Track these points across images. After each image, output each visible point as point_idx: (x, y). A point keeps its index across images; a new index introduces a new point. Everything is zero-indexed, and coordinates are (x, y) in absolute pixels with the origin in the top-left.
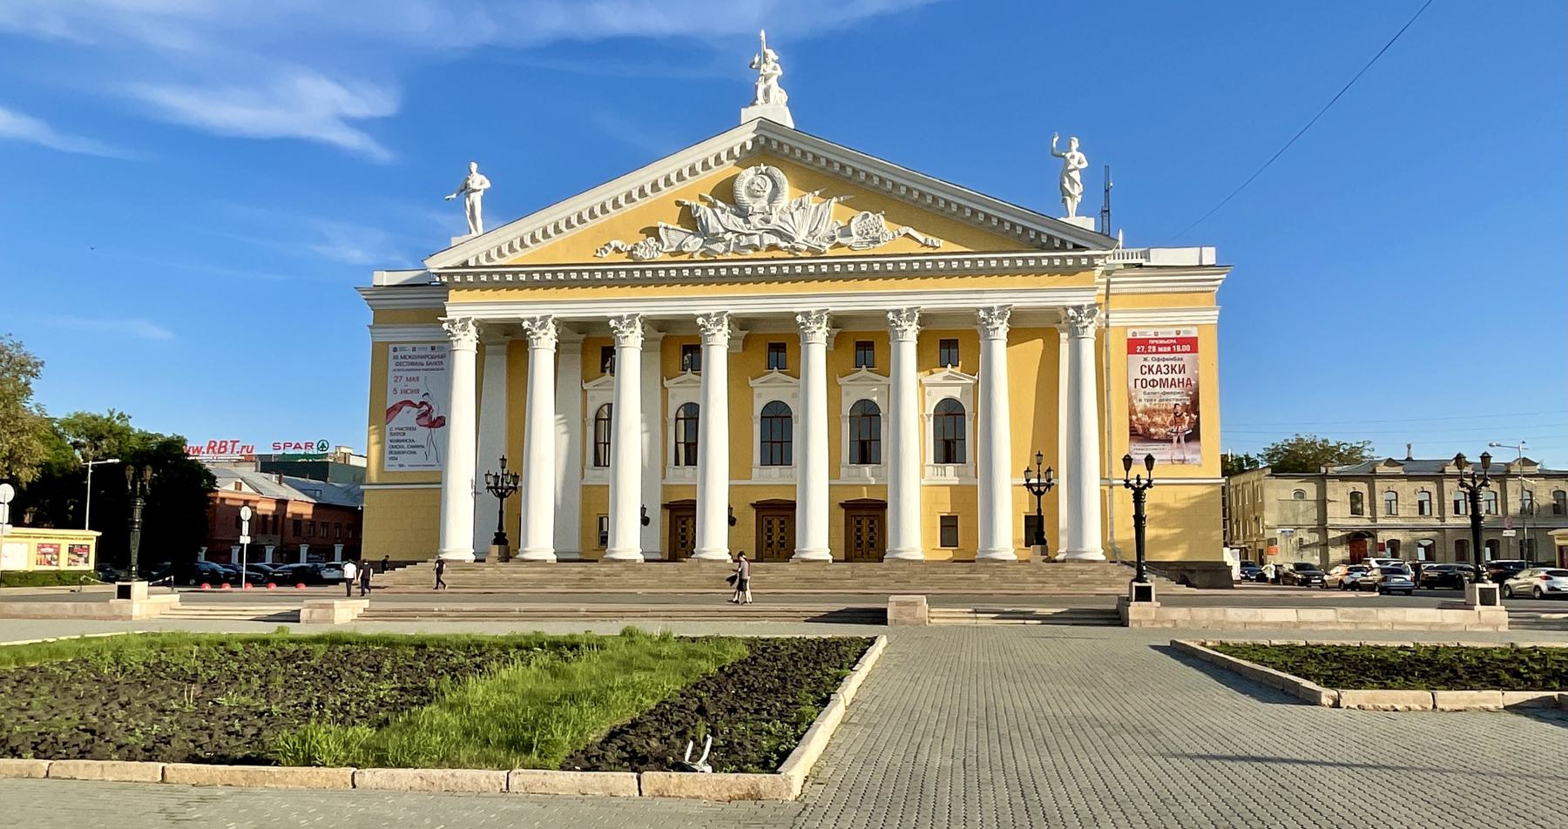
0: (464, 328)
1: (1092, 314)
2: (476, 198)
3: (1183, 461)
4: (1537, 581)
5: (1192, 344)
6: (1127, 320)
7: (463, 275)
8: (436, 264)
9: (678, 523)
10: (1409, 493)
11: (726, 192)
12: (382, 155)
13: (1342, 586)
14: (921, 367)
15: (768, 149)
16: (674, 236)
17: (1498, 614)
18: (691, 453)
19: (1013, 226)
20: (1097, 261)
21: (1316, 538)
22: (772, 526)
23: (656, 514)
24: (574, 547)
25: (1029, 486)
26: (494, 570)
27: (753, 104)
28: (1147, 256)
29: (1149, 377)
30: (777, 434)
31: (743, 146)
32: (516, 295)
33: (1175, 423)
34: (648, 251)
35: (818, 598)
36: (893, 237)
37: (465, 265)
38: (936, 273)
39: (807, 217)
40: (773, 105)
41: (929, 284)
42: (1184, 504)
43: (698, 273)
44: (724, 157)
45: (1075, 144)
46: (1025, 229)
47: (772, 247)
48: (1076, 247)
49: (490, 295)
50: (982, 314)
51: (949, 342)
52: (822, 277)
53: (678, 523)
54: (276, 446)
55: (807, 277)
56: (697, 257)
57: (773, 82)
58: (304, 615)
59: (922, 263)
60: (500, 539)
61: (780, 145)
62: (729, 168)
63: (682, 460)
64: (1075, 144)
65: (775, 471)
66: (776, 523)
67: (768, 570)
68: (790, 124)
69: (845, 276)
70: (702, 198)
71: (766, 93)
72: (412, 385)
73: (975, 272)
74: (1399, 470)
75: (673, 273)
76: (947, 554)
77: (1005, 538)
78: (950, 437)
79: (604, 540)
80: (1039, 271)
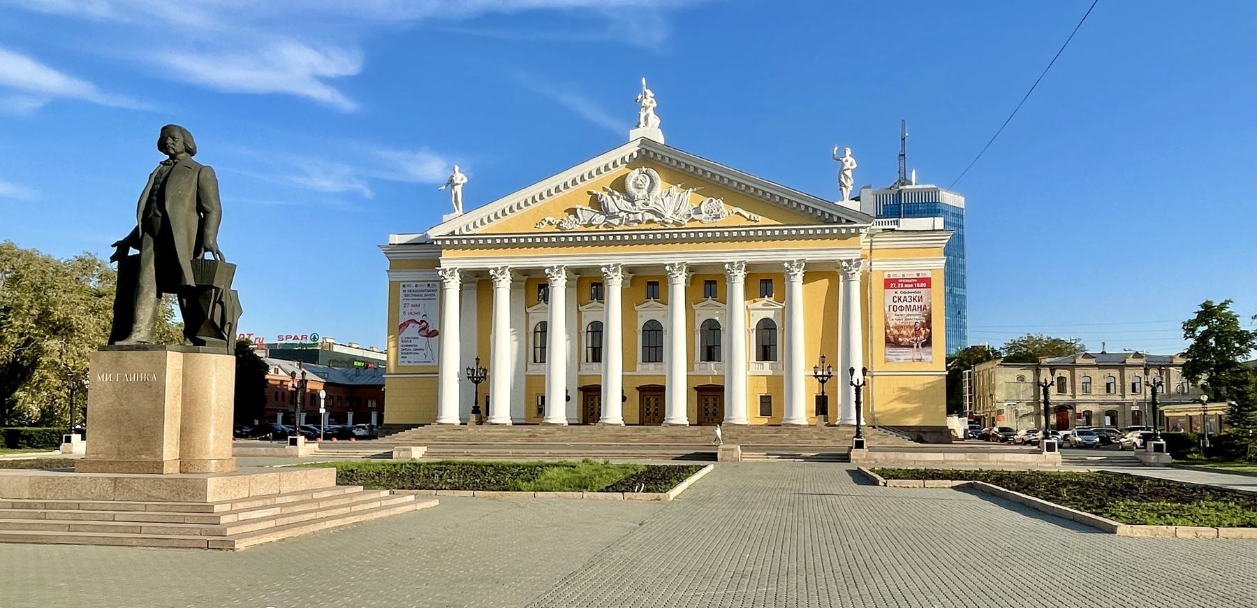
0: (452, 274)
1: (858, 265)
2: (458, 189)
3: (920, 360)
4: (1135, 440)
5: (927, 282)
6: (884, 266)
7: (451, 240)
8: (433, 233)
9: (589, 399)
10: (1099, 378)
11: (620, 185)
12: (347, 105)
13: (1025, 443)
14: (747, 297)
15: (647, 157)
16: (586, 214)
17: (1056, 456)
18: (597, 354)
19: (807, 207)
20: (862, 231)
21: (1032, 409)
22: (649, 402)
23: (575, 395)
24: (522, 416)
25: (816, 377)
26: (472, 430)
27: (638, 127)
28: (897, 223)
29: (898, 304)
30: (652, 342)
31: (631, 155)
32: (485, 253)
33: (915, 335)
34: (570, 224)
35: (679, 447)
36: (728, 214)
37: (453, 233)
38: (756, 239)
39: (672, 201)
40: (651, 129)
41: (753, 245)
42: (920, 388)
43: (602, 238)
44: (619, 162)
45: (848, 152)
46: (814, 210)
47: (650, 221)
48: (848, 221)
49: (468, 253)
50: (786, 265)
51: (766, 282)
52: (682, 241)
53: (589, 399)
54: (280, 338)
55: (672, 241)
56: (601, 228)
57: (650, 111)
58: (395, 454)
59: (747, 232)
60: (476, 410)
61: (655, 154)
62: (622, 169)
63: (590, 359)
64: (848, 152)
65: (651, 366)
66: (652, 400)
67: (648, 431)
68: (661, 140)
69: (697, 240)
70: (605, 189)
71: (646, 118)
72: (416, 310)
73: (782, 238)
74: (1092, 361)
75: (586, 239)
76: (765, 420)
77: (801, 411)
78: (766, 343)
79: (541, 411)
80: (823, 237)
